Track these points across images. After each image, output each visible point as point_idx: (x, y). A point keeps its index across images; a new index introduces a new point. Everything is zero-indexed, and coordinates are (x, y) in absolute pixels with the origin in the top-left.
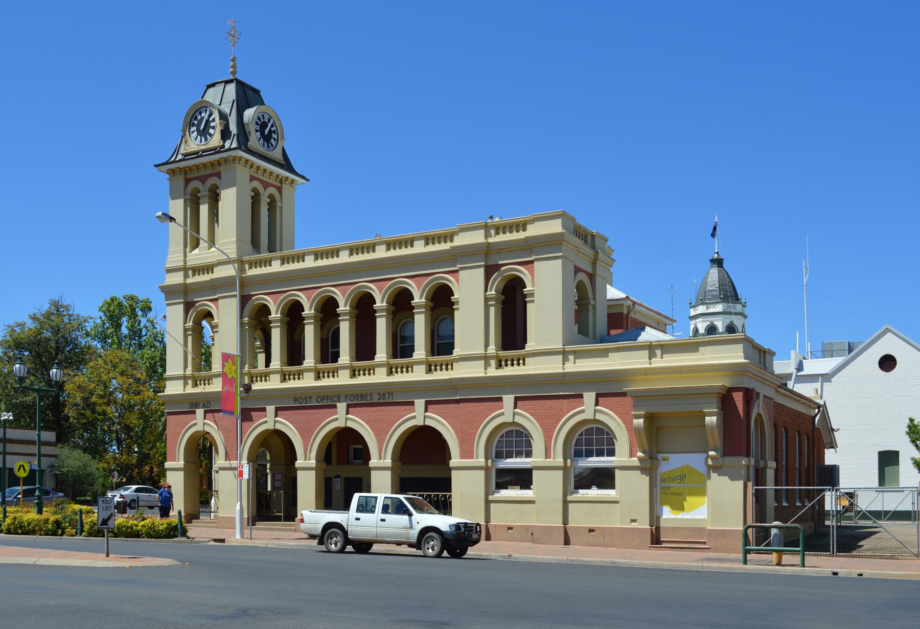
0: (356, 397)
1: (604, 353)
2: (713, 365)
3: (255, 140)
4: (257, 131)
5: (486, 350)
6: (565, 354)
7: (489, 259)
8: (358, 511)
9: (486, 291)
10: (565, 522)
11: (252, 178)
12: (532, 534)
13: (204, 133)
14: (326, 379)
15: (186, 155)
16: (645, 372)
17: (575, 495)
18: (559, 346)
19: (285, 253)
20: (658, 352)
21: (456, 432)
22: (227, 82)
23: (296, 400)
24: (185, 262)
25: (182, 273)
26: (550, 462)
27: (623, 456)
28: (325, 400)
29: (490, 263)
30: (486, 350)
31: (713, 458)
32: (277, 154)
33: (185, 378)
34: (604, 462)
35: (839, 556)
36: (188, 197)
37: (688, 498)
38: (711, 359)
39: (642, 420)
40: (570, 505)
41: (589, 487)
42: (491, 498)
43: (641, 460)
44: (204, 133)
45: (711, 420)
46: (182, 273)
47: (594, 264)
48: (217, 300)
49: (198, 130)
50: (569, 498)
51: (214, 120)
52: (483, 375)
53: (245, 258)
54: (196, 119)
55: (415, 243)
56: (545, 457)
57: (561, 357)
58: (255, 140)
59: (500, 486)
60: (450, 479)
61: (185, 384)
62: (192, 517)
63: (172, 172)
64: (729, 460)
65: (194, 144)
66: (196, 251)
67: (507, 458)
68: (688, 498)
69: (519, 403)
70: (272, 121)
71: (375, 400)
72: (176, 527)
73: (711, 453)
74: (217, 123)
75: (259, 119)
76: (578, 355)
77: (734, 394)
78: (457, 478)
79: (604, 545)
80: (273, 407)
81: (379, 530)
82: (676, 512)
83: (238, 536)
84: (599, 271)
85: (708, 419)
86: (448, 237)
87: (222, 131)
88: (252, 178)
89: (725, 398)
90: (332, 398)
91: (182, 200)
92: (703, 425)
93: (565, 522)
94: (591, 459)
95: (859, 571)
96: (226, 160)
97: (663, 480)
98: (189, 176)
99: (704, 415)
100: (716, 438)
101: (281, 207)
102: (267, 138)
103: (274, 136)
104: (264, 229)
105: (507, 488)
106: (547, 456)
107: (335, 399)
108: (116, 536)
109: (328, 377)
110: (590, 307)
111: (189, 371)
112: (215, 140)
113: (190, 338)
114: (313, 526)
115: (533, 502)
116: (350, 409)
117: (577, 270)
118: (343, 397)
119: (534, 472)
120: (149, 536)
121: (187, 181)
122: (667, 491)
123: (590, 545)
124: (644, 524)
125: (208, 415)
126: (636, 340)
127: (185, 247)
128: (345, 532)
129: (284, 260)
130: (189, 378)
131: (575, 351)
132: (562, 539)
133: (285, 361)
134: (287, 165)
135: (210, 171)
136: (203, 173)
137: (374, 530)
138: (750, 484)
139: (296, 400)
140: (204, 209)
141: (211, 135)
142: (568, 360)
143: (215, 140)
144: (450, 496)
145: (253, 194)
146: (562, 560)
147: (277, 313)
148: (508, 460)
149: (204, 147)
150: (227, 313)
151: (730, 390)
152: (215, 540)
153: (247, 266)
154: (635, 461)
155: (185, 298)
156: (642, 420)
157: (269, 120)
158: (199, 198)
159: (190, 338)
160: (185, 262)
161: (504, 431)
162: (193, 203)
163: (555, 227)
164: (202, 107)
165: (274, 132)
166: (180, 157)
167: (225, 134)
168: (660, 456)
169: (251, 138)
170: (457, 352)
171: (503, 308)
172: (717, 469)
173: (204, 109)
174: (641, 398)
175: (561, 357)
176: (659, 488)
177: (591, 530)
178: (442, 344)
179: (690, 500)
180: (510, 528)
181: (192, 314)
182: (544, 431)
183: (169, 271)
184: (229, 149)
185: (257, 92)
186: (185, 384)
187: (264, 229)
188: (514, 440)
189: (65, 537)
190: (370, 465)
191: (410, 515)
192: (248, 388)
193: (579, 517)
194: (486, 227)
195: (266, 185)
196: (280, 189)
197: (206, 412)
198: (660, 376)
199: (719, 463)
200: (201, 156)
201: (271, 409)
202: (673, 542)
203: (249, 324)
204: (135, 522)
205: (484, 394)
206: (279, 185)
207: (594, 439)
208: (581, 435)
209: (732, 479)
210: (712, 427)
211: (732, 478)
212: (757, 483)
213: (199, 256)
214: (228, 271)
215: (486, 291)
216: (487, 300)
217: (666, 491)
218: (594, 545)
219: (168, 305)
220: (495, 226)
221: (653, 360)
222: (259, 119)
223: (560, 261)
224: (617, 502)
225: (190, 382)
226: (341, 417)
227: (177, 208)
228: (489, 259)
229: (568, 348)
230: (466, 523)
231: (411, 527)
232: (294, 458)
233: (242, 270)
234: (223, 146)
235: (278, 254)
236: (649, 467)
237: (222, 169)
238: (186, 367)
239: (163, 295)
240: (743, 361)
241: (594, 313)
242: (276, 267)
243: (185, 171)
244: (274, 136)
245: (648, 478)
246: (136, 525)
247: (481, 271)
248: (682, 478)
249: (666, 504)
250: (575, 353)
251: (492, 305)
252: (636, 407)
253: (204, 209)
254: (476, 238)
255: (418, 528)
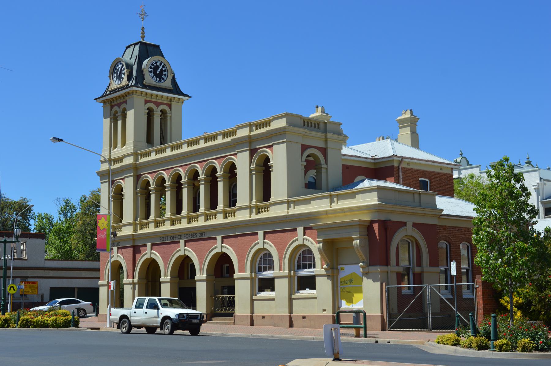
0: (192, 235)
1: (307, 202)
2: (360, 207)
3: (149, 79)
4: (151, 72)
5: (250, 203)
6: (288, 203)
7: (251, 145)
8: (147, 308)
9: (250, 165)
10: (291, 312)
11: (146, 102)
12: (273, 320)
13: (119, 77)
14: (264, 213)
15: (111, 91)
16: (326, 213)
17: (298, 294)
18: (285, 198)
19: (174, 143)
20: (335, 199)
21: (237, 256)
22: (136, 44)
23: (161, 239)
24: (110, 156)
25: (248, 129)
26: (282, 273)
27: (318, 269)
28: (172, 239)
29: (253, 148)
30: (250, 203)
31: (362, 267)
32: (167, 84)
33: (250, 208)
34: (311, 272)
35: (433, 332)
36: (112, 116)
37: (355, 295)
38: (362, 202)
39: (321, 244)
40: (294, 301)
41: (305, 289)
42: (254, 297)
43: (326, 269)
44: (119, 77)
45: (356, 242)
46: (248, 129)
47: (326, 141)
48: (271, 146)
49: (117, 76)
50: (293, 296)
51: (124, 69)
52: (248, 219)
53: (139, 152)
54: (114, 71)
55: (152, 154)
56: (279, 271)
57: (286, 205)
58: (149, 79)
59: (261, 289)
60: (195, 288)
61: (251, 213)
62: (211, 316)
63: (104, 102)
64: (372, 268)
65: (115, 85)
66: (116, 150)
67: (264, 271)
68: (355, 295)
69: (267, 236)
70: (163, 64)
71: (198, 237)
72: (70, 321)
73: (361, 264)
74: (125, 72)
75: (152, 64)
76: (296, 203)
77: (374, 225)
78: (237, 284)
79: (310, 327)
80: (263, 231)
81: (144, 319)
82: (349, 304)
83: (108, 326)
84: (330, 145)
85: (354, 242)
86: (233, 133)
87: (128, 75)
88: (146, 102)
89: (368, 227)
90: (178, 238)
91: (109, 119)
92: (352, 247)
93: (291, 312)
94: (305, 270)
95: (388, 340)
96: (128, 93)
97: (342, 283)
98: (113, 104)
99: (353, 239)
100: (362, 254)
101: (171, 116)
102: (159, 76)
103: (164, 73)
104: (157, 130)
105: (264, 291)
106: (280, 270)
107: (179, 237)
108: (35, 327)
109: (265, 211)
110: (323, 170)
111: (254, 202)
112: (125, 82)
113: (254, 176)
114: (115, 317)
115: (273, 300)
116: (187, 243)
117: (304, 148)
118: (183, 236)
119: (276, 280)
120: (53, 327)
121: (112, 107)
122: (344, 290)
123: (304, 327)
124: (285, 312)
125: (120, 250)
126: (235, 205)
127: (111, 147)
128: (129, 321)
129: (173, 148)
130: (253, 207)
131: (294, 201)
132: (379, 326)
133: (209, 206)
134: (176, 89)
135: (122, 100)
136: (119, 101)
137: (141, 319)
138: (384, 284)
139: (161, 239)
140: (120, 123)
141: (163, 79)
142: (291, 207)
143: (125, 82)
144: (234, 297)
145: (148, 111)
146: (249, 336)
147: (202, 175)
148: (265, 273)
149: (119, 86)
150: (128, 185)
151: (372, 222)
152: (91, 329)
153: (139, 157)
154: (323, 272)
155: (250, 146)
156: (321, 244)
157: (161, 64)
158: (117, 117)
159: (254, 176)
160: (110, 156)
161: (261, 255)
162: (114, 121)
163: (281, 123)
164: (117, 62)
165: (165, 71)
166: (108, 93)
167: (129, 78)
168: (340, 267)
169: (145, 78)
170: (238, 205)
171: (211, 185)
172: (365, 274)
173: (119, 63)
174: (322, 230)
175: (286, 205)
176: (339, 288)
177: (304, 317)
178: (232, 200)
179: (356, 296)
180: (263, 317)
181: (256, 157)
182: (279, 253)
183: (102, 162)
184: (131, 86)
185: (158, 47)
186: (251, 213)
187: (157, 130)
188: (264, 260)
189: (9, 328)
190: (196, 279)
191: (158, 309)
192: (114, 234)
193: (299, 309)
194: (250, 125)
195: (158, 104)
196: (170, 106)
197: (118, 249)
198: (335, 215)
199: (366, 271)
200: (118, 91)
201: (261, 233)
202: (347, 324)
203: (140, 192)
204: (48, 318)
205: (246, 230)
206: (169, 103)
207: (304, 258)
208: (300, 255)
209: (374, 281)
210: (357, 247)
211: (374, 281)
212: (388, 284)
213: (117, 152)
214: (129, 161)
215: (250, 165)
216: (251, 171)
217: (342, 289)
218: (306, 327)
219: (102, 183)
220: (255, 124)
221: (333, 204)
222: (152, 64)
223: (285, 144)
224: (316, 298)
225: (254, 210)
226: (220, 246)
227: (107, 122)
228: (251, 145)
229: (290, 199)
230: (187, 314)
231: (158, 317)
232: (195, 274)
233: (136, 160)
234: (128, 85)
235: (169, 144)
236: (333, 272)
237: (126, 98)
238: (251, 199)
239: (99, 177)
240: (377, 203)
241: (327, 173)
242: (169, 153)
243: (111, 101)
244: (164, 73)
245: (330, 282)
246: (47, 321)
247: (247, 153)
248: (351, 281)
249: (343, 299)
250: (294, 202)
251: (254, 174)
252: (319, 236)
253: (120, 123)
254: (243, 133)
255: (161, 317)
